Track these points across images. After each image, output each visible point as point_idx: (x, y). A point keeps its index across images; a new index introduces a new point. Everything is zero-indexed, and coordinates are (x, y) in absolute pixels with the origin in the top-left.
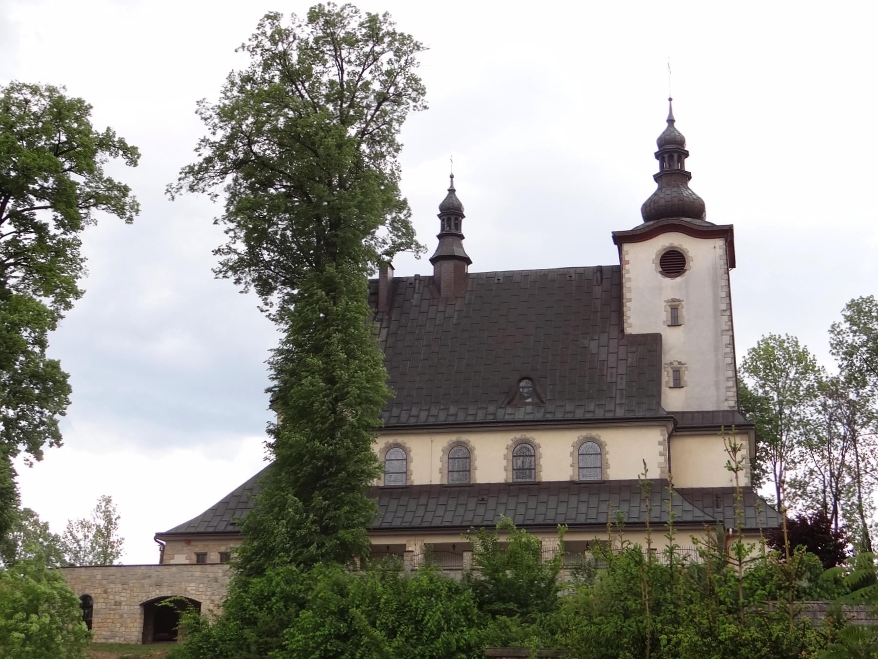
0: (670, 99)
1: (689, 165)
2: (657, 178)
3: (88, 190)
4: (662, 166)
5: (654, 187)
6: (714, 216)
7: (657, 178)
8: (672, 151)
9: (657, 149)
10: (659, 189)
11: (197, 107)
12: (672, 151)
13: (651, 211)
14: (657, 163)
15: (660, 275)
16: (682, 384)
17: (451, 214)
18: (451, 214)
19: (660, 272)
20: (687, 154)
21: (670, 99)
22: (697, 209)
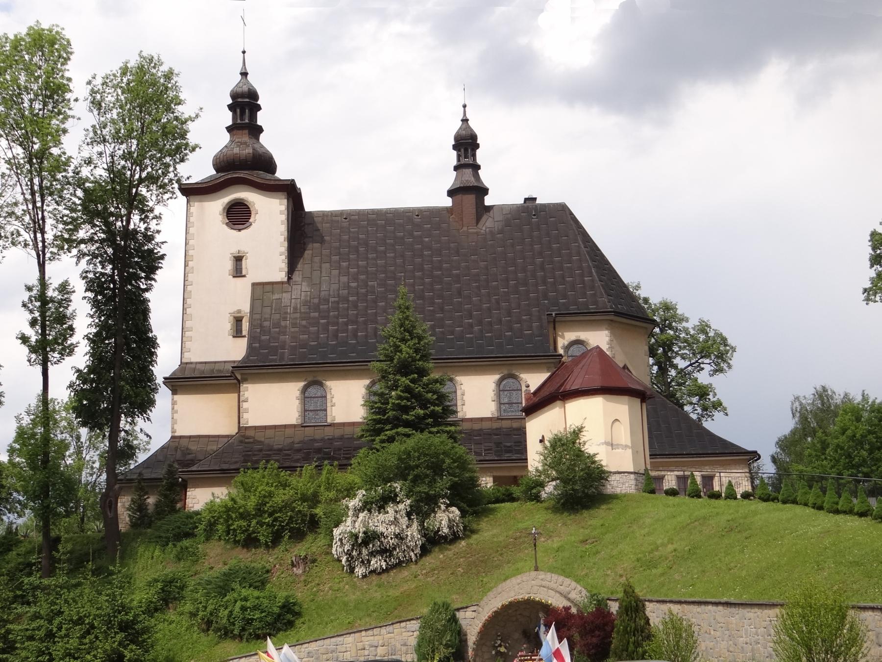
0: (244, 52)
1: (261, 119)
2: (229, 129)
3: (114, 114)
4: (234, 118)
5: (226, 138)
6: (282, 173)
7: (229, 129)
8: (466, 144)
9: (230, 101)
10: (232, 141)
11: (90, 87)
12: (466, 144)
13: (223, 164)
14: (230, 114)
15: (225, 226)
16: (244, 273)
17: (245, 106)
18: (245, 106)
19: (227, 224)
20: (259, 108)
21: (244, 52)
22: (266, 163)
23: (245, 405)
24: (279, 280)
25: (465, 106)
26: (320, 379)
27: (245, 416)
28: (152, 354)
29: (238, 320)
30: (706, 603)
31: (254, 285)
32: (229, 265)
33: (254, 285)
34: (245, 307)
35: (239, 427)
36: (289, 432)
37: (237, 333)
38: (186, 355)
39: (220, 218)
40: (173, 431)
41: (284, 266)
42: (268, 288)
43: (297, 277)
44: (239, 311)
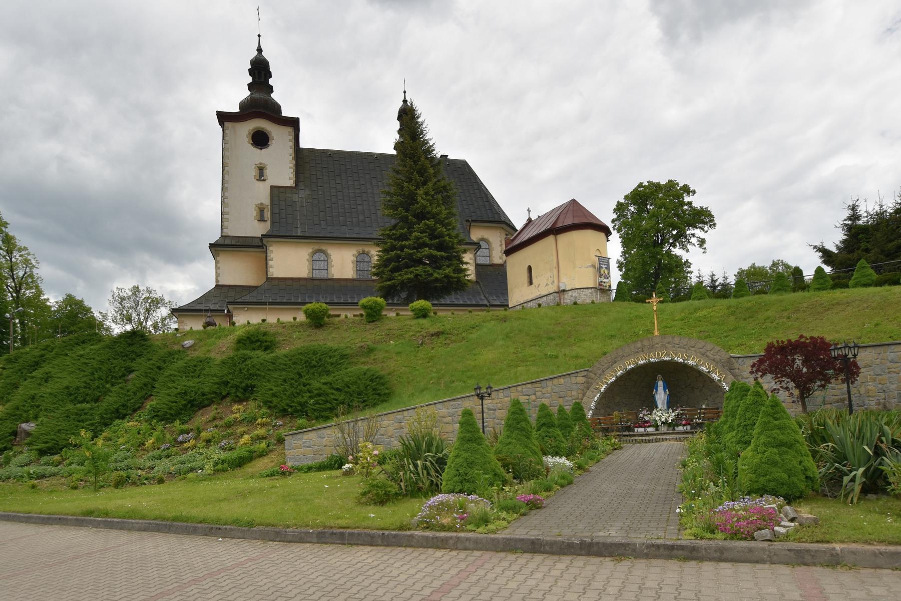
20: (82, 301)
21: (259, 36)
23: (270, 263)
24: (289, 185)
25: (405, 92)
26: (323, 248)
27: (271, 270)
28: (425, 142)
29: (261, 211)
30: (265, 303)
31: (272, 188)
32: (254, 172)
33: (272, 188)
34: (267, 201)
35: (267, 279)
36: (302, 283)
37: (261, 219)
38: (225, 230)
39: (247, 139)
40: (217, 281)
41: (292, 176)
42: (282, 190)
43: (302, 186)
44: (262, 204)
